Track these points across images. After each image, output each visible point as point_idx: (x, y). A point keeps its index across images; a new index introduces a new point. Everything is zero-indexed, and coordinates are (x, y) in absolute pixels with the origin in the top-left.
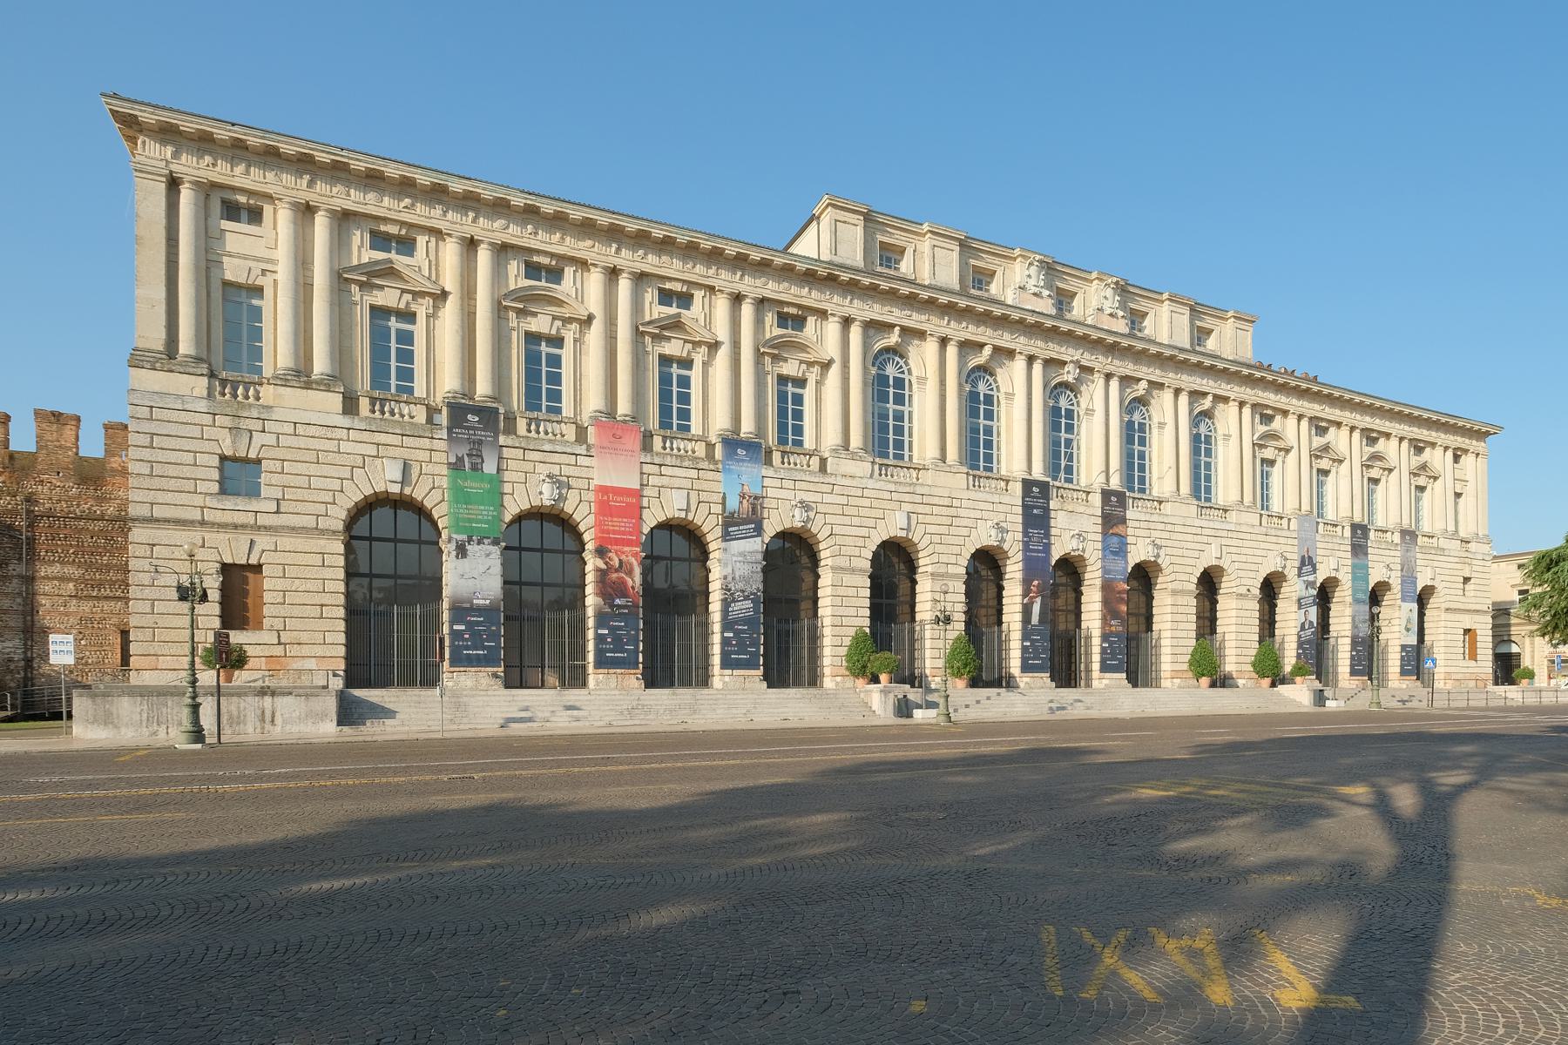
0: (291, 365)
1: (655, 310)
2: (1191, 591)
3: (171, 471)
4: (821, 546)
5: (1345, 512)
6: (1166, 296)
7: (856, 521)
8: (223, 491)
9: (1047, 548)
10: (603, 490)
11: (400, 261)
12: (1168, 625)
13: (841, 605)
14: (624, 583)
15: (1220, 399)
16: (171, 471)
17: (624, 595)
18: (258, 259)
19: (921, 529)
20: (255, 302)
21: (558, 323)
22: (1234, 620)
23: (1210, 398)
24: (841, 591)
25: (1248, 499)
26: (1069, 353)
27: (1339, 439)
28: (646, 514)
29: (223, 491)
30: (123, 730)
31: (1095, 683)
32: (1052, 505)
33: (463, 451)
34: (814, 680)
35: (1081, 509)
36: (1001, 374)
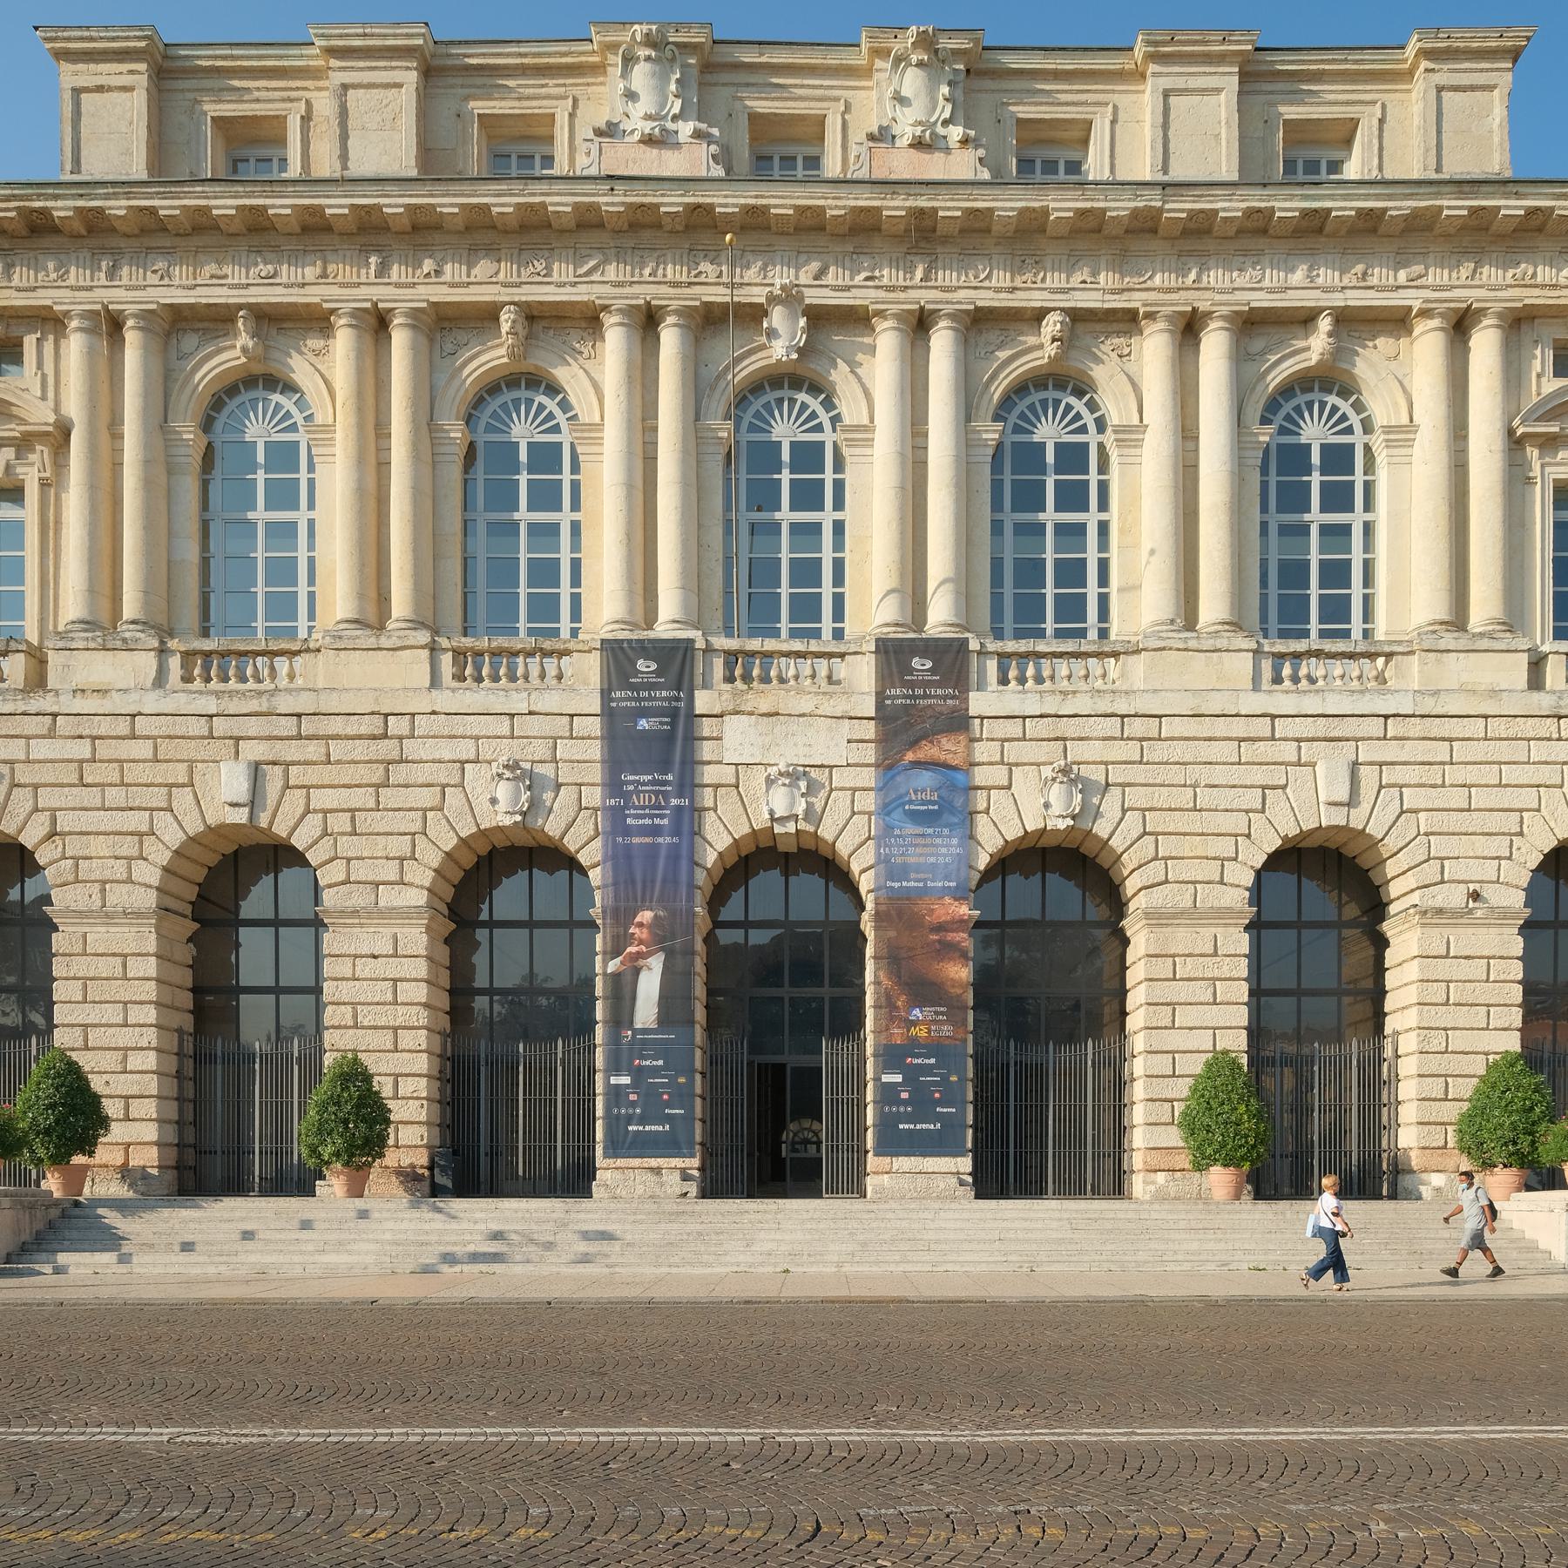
0: (1226, 616)
4: (1391, 868)
7: (115, 796)
9: (689, 822)
13: (1183, 1005)
19: (295, 800)
23: (1325, 324)
24: (1443, 969)
25: (1484, 605)
26: (759, 281)
28: (983, 825)
32: (703, 701)
34: (1115, 1185)
35: (806, 704)
36: (1105, 375)
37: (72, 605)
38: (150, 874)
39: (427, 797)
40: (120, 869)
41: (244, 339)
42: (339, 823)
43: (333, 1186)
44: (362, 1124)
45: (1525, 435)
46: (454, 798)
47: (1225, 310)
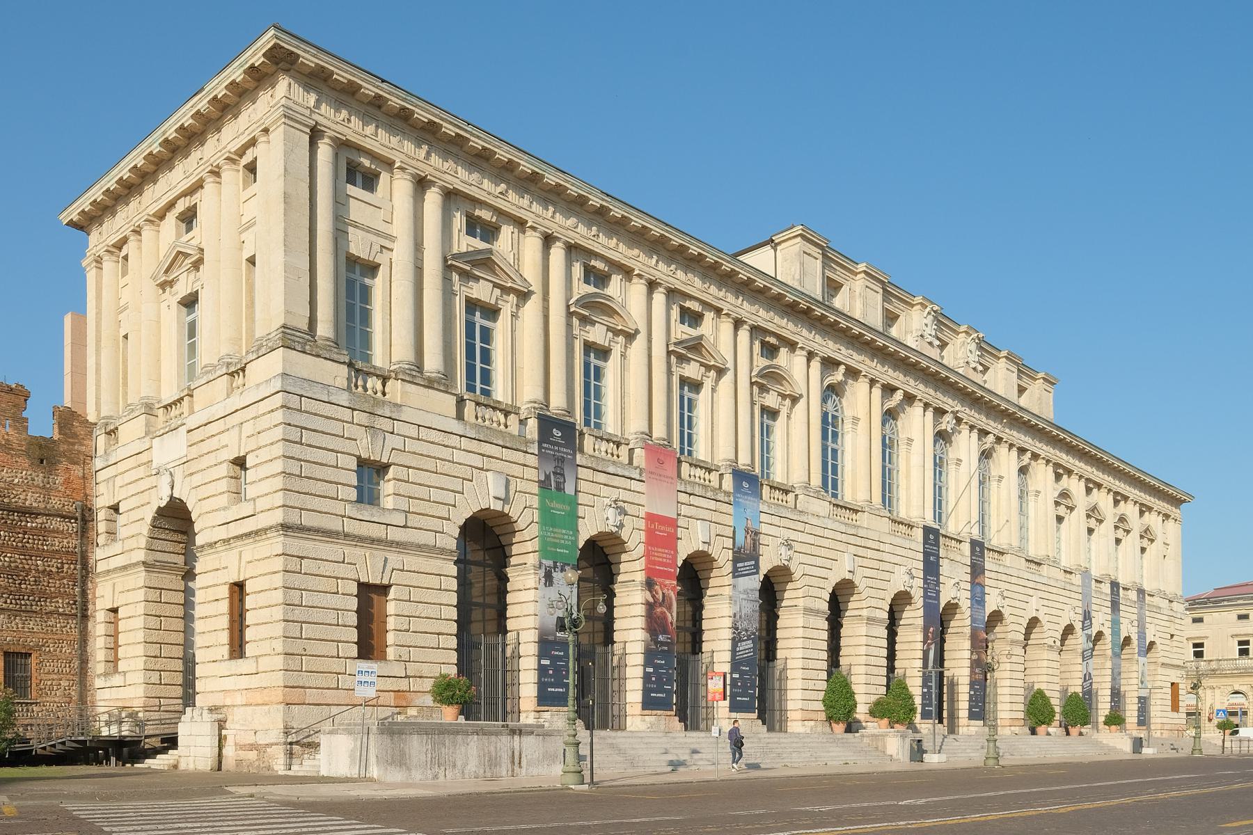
1: (464, 243)
2: (824, 613)
3: (319, 472)
5: (723, 453)
6: (1004, 353)
8: (360, 500)
9: (937, 598)
10: (651, 518)
12: (799, 653)
14: (665, 618)
15: (853, 373)
16: (319, 472)
17: (665, 632)
18: (378, 234)
20: (367, 281)
21: (497, 292)
22: (799, 643)
27: (718, 334)
30: (413, 772)
31: (962, 730)
33: (550, 469)
45: (452, 265)
47: (411, 170)
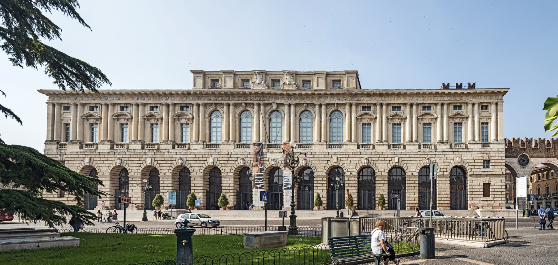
7: (198, 162)
8: (484, 167)
11: (399, 112)
19: (218, 162)
29: (484, 167)
37: (408, 139)
38: (325, 171)
39: (233, 162)
40: (198, 171)
41: (214, 107)
42: (223, 165)
43: (221, 209)
44: (225, 202)
46: (236, 162)
